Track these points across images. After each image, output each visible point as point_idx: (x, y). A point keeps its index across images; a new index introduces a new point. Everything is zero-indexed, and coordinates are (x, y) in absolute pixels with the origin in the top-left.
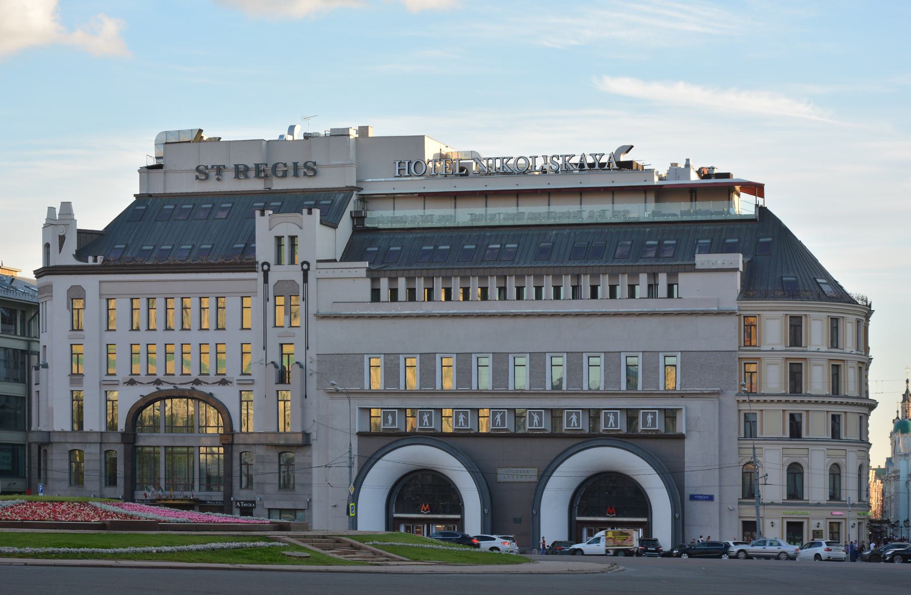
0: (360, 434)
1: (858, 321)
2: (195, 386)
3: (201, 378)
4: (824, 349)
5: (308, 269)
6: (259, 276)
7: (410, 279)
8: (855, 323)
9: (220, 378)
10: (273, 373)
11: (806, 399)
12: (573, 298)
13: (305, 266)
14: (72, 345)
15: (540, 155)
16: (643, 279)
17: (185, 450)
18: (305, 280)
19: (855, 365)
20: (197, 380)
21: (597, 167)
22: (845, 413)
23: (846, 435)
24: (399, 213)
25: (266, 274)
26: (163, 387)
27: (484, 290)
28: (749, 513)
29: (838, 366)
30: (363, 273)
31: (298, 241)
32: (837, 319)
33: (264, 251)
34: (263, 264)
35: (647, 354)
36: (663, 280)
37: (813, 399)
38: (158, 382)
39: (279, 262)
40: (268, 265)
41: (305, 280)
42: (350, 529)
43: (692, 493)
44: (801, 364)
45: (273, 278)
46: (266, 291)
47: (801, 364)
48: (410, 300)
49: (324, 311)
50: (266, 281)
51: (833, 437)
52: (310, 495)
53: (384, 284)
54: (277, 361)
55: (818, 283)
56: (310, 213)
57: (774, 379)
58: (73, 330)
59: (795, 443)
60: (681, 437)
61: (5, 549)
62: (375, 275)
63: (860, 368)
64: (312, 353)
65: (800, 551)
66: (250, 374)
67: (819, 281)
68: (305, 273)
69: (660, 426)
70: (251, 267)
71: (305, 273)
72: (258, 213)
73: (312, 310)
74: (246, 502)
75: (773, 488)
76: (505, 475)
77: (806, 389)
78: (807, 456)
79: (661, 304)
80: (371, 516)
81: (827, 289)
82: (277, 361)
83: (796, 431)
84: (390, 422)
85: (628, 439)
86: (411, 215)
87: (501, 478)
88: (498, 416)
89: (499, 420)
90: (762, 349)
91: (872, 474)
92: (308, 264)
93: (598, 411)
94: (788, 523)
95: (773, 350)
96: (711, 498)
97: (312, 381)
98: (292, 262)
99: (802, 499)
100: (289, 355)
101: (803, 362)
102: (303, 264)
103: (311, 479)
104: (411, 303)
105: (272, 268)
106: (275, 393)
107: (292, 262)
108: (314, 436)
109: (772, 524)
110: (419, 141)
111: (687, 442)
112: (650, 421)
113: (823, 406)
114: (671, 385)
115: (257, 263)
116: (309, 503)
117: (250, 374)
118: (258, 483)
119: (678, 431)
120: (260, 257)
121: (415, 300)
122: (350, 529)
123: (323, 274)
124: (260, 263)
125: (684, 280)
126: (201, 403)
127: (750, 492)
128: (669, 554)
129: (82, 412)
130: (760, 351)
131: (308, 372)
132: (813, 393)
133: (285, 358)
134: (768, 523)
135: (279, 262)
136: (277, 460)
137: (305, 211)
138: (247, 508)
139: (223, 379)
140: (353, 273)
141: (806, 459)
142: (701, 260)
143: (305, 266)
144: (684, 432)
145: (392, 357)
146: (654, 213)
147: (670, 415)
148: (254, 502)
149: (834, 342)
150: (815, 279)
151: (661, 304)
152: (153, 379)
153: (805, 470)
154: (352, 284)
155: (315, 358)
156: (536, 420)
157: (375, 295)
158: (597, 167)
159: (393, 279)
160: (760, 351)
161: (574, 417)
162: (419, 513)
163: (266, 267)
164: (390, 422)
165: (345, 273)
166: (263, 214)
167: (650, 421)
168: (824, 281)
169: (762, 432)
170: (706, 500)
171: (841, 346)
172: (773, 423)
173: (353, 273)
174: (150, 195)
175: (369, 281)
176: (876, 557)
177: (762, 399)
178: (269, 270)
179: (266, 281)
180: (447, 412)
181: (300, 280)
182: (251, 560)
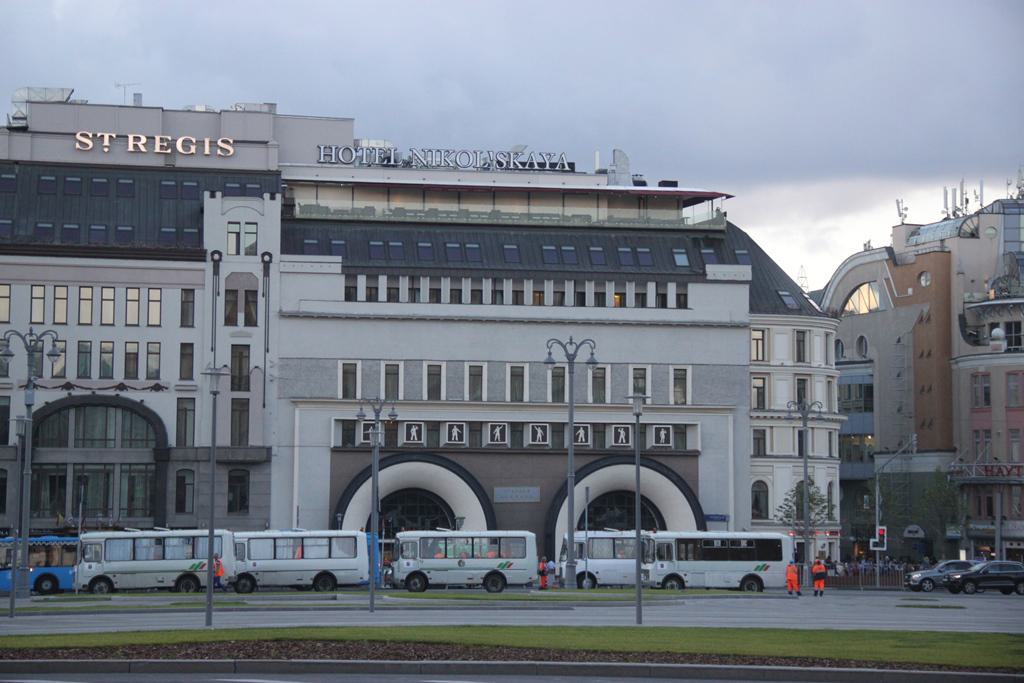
1: (827, 335)
2: (118, 392)
3: (128, 383)
4: (790, 363)
5: (270, 261)
6: (208, 266)
7: (413, 279)
8: (823, 337)
9: (152, 383)
11: (769, 415)
12: (389, 300)
13: (267, 258)
17: (102, 467)
18: (266, 273)
20: (122, 384)
21: (548, 167)
23: (813, 451)
24: (323, 203)
25: (216, 265)
26: (76, 392)
27: (623, 296)
29: (804, 380)
30: (338, 268)
32: (803, 332)
34: (213, 253)
37: (776, 415)
38: (68, 386)
41: (266, 273)
43: (751, 517)
45: (225, 270)
47: (356, 365)
48: (621, 306)
49: (289, 308)
50: (216, 272)
53: (362, 282)
55: (780, 296)
56: (273, 198)
57: (782, 394)
59: (760, 461)
60: (695, 454)
62: (352, 271)
63: (829, 382)
64: (272, 356)
67: (781, 293)
68: (266, 266)
70: (200, 256)
71: (266, 266)
72: (207, 194)
73: (274, 309)
77: (770, 405)
78: (772, 474)
79: (672, 314)
81: (789, 301)
83: (760, 450)
86: (336, 204)
88: (498, 430)
89: (498, 434)
90: (772, 363)
92: (270, 255)
95: (782, 365)
99: (767, 518)
101: (767, 377)
102: (263, 255)
104: (599, 308)
106: (150, 328)
108: (275, 451)
111: (701, 460)
112: (663, 437)
115: (206, 251)
119: (690, 447)
120: (209, 244)
121: (522, 304)
123: (289, 267)
124: (209, 252)
125: (695, 291)
126: (112, 411)
130: (770, 366)
132: (777, 408)
137: (267, 196)
139: (157, 384)
140: (326, 268)
141: (771, 477)
142: (713, 270)
143: (267, 258)
144: (700, 449)
146: (610, 218)
147: (681, 431)
149: (800, 356)
150: (777, 292)
151: (672, 314)
152: (62, 382)
153: (770, 489)
155: (276, 361)
156: (539, 435)
157: (350, 295)
158: (548, 167)
159: (372, 277)
160: (770, 366)
163: (216, 257)
165: (317, 268)
166: (213, 196)
167: (663, 437)
168: (787, 293)
169: (772, 450)
170: (721, 520)
171: (807, 360)
172: (783, 440)
173: (326, 268)
174: (17, 162)
175: (342, 278)
176: (543, 588)
177: (769, 415)
178: (220, 260)
179: (216, 272)
181: (259, 274)
182: (38, 608)
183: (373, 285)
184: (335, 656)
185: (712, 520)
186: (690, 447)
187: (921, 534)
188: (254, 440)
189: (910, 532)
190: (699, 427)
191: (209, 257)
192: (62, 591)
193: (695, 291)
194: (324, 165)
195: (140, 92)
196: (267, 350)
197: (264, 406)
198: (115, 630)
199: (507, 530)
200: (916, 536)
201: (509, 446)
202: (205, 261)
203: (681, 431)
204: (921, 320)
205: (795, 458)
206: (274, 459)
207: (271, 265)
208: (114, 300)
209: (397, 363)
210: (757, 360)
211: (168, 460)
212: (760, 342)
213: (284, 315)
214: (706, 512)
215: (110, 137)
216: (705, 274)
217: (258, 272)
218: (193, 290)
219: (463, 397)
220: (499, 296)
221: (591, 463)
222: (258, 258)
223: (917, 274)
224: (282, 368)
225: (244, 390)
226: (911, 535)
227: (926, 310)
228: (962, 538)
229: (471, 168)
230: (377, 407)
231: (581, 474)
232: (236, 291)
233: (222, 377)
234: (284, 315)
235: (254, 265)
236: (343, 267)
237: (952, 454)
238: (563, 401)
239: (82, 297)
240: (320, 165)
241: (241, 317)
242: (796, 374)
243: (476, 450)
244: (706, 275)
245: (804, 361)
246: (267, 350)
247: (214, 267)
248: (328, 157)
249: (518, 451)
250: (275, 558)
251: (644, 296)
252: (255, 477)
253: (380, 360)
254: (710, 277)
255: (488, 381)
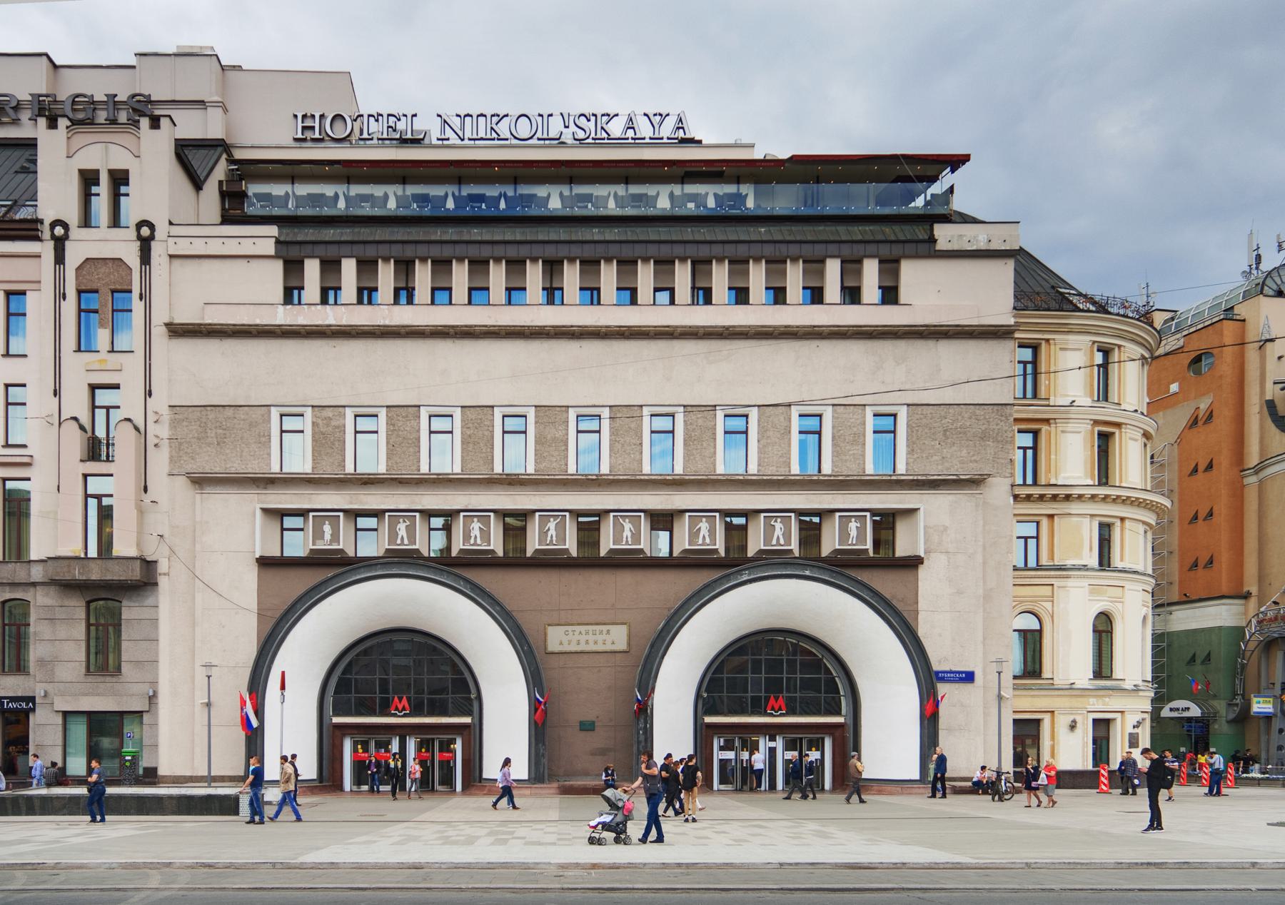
0: (265, 563)
5: (152, 237)
6: (46, 249)
10: (74, 443)
13: (145, 231)
14: (85, 476)
15: (556, 113)
16: (833, 269)
18: (145, 258)
19: (1138, 435)
22: (1122, 519)
23: (1122, 560)
25: (60, 244)
28: (1029, 703)
30: (269, 247)
31: (968, 686)
33: (55, 196)
34: (54, 224)
35: (467, 411)
36: (871, 272)
39: (86, 222)
40: (66, 226)
41: (145, 258)
42: (236, 813)
44: (1038, 721)
45: (75, 253)
46: (59, 281)
50: (60, 259)
51: (1101, 564)
52: (154, 683)
54: (85, 420)
55: (1062, 294)
58: (79, 350)
59: (1106, 578)
60: (913, 563)
61: (4, 838)
62: (294, 252)
64: (159, 403)
65: (1009, 481)
66: (24, 446)
69: (496, 544)
70: (29, 230)
73: (160, 316)
74: (12, 699)
75: (1070, 657)
76: (559, 639)
78: (1051, 599)
79: (870, 313)
80: (293, 730)
82: (85, 420)
84: (328, 536)
85: (811, 560)
87: (553, 646)
89: (552, 532)
90: (273, 230)
91: (730, 189)
92: (151, 226)
93: (525, 515)
94: (1095, 721)
96: (969, 677)
97: (160, 462)
98: (115, 222)
100: (108, 408)
103: (157, 654)
105: (75, 232)
106: (81, 478)
107: (115, 222)
108: (163, 567)
109: (1073, 727)
110: (98, 184)
111: (922, 571)
112: (853, 533)
113: (1043, 505)
114: (827, 468)
115: (41, 222)
116: (152, 699)
117: (24, 446)
118: (42, 662)
121: (784, 303)
122: (236, 813)
123: (183, 247)
125: (912, 273)
127: (1032, 668)
128: (987, 787)
129: (17, 812)
131: (151, 440)
133: (100, 414)
134: (1063, 721)
135: (86, 222)
136: (83, 615)
138: (16, 711)
140: (247, 248)
141: (1048, 605)
145: (328, 413)
147: (886, 522)
148: (32, 699)
154: (246, 280)
155: (165, 411)
156: (627, 533)
157: (291, 293)
161: (704, 526)
162: (766, 714)
163: (59, 231)
164: (328, 536)
167: (853, 533)
170: (962, 680)
175: (278, 266)
179: (60, 259)
180: (814, 755)
181: (133, 260)
182: (472, 590)
183: (293, 284)
184: (559, 434)
185: (942, 680)
186: (902, 548)
187: (1195, 711)
188: (123, 546)
189: (1171, 710)
190: (921, 512)
191: (46, 234)
192: (224, 75)
193: (912, 273)
194: (304, 145)
195: (583, 734)
196: (149, 393)
197: (146, 490)
198: (1111, 859)
199: (148, 814)
200: (1186, 714)
201: (797, 555)
202: (37, 239)
203: (886, 522)
204: (1194, 422)
205: (1093, 569)
206: (163, 582)
207: (153, 244)
208: (357, 530)
209: (722, 787)
210: (1025, 484)
211: (627, 183)
212: (1032, 543)
213: (178, 331)
214: (936, 667)
215: (722, 749)
216: (933, 240)
217: (131, 255)
218: (23, 293)
219: (269, 465)
220: (403, 294)
221: (715, 581)
222: (132, 234)
223: (1037, 609)
224: (174, 424)
225: (156, 627)
226: (1175, 714)
227: (1203, 406)
228: (1275, 715)
229: (534, 141)
230: (630, 133)
231: (401, 562)
232: (1159, 827)
233: (1069, 353)
234: (178, 331)
235: (124, 247)
236: (278, 242)
237: (1242, 602)
238: (336, 714)
239: (12, 311)
240: (298, 145)
241: (366, 301)
242: (1096, 422)
243: (515, 561)
244: (935, 241)
245: (1109, 677)
246: (149, 393)
247: (56, 249)
248: (309, 131)
249: (589, 560)
250: (652, 432)
251: (634, 291)
252: (130, 611)
253: (789, 405)
254: (942, 245)
255: (537, 442)
